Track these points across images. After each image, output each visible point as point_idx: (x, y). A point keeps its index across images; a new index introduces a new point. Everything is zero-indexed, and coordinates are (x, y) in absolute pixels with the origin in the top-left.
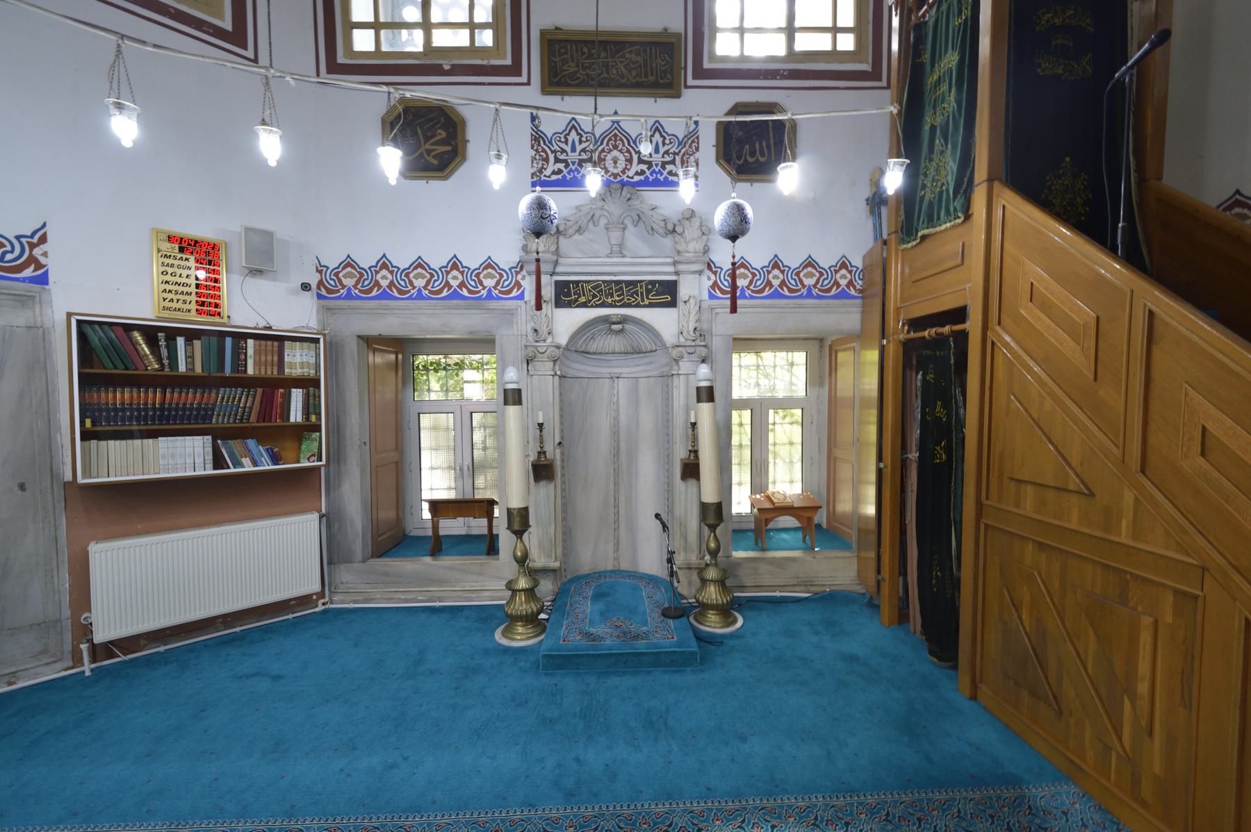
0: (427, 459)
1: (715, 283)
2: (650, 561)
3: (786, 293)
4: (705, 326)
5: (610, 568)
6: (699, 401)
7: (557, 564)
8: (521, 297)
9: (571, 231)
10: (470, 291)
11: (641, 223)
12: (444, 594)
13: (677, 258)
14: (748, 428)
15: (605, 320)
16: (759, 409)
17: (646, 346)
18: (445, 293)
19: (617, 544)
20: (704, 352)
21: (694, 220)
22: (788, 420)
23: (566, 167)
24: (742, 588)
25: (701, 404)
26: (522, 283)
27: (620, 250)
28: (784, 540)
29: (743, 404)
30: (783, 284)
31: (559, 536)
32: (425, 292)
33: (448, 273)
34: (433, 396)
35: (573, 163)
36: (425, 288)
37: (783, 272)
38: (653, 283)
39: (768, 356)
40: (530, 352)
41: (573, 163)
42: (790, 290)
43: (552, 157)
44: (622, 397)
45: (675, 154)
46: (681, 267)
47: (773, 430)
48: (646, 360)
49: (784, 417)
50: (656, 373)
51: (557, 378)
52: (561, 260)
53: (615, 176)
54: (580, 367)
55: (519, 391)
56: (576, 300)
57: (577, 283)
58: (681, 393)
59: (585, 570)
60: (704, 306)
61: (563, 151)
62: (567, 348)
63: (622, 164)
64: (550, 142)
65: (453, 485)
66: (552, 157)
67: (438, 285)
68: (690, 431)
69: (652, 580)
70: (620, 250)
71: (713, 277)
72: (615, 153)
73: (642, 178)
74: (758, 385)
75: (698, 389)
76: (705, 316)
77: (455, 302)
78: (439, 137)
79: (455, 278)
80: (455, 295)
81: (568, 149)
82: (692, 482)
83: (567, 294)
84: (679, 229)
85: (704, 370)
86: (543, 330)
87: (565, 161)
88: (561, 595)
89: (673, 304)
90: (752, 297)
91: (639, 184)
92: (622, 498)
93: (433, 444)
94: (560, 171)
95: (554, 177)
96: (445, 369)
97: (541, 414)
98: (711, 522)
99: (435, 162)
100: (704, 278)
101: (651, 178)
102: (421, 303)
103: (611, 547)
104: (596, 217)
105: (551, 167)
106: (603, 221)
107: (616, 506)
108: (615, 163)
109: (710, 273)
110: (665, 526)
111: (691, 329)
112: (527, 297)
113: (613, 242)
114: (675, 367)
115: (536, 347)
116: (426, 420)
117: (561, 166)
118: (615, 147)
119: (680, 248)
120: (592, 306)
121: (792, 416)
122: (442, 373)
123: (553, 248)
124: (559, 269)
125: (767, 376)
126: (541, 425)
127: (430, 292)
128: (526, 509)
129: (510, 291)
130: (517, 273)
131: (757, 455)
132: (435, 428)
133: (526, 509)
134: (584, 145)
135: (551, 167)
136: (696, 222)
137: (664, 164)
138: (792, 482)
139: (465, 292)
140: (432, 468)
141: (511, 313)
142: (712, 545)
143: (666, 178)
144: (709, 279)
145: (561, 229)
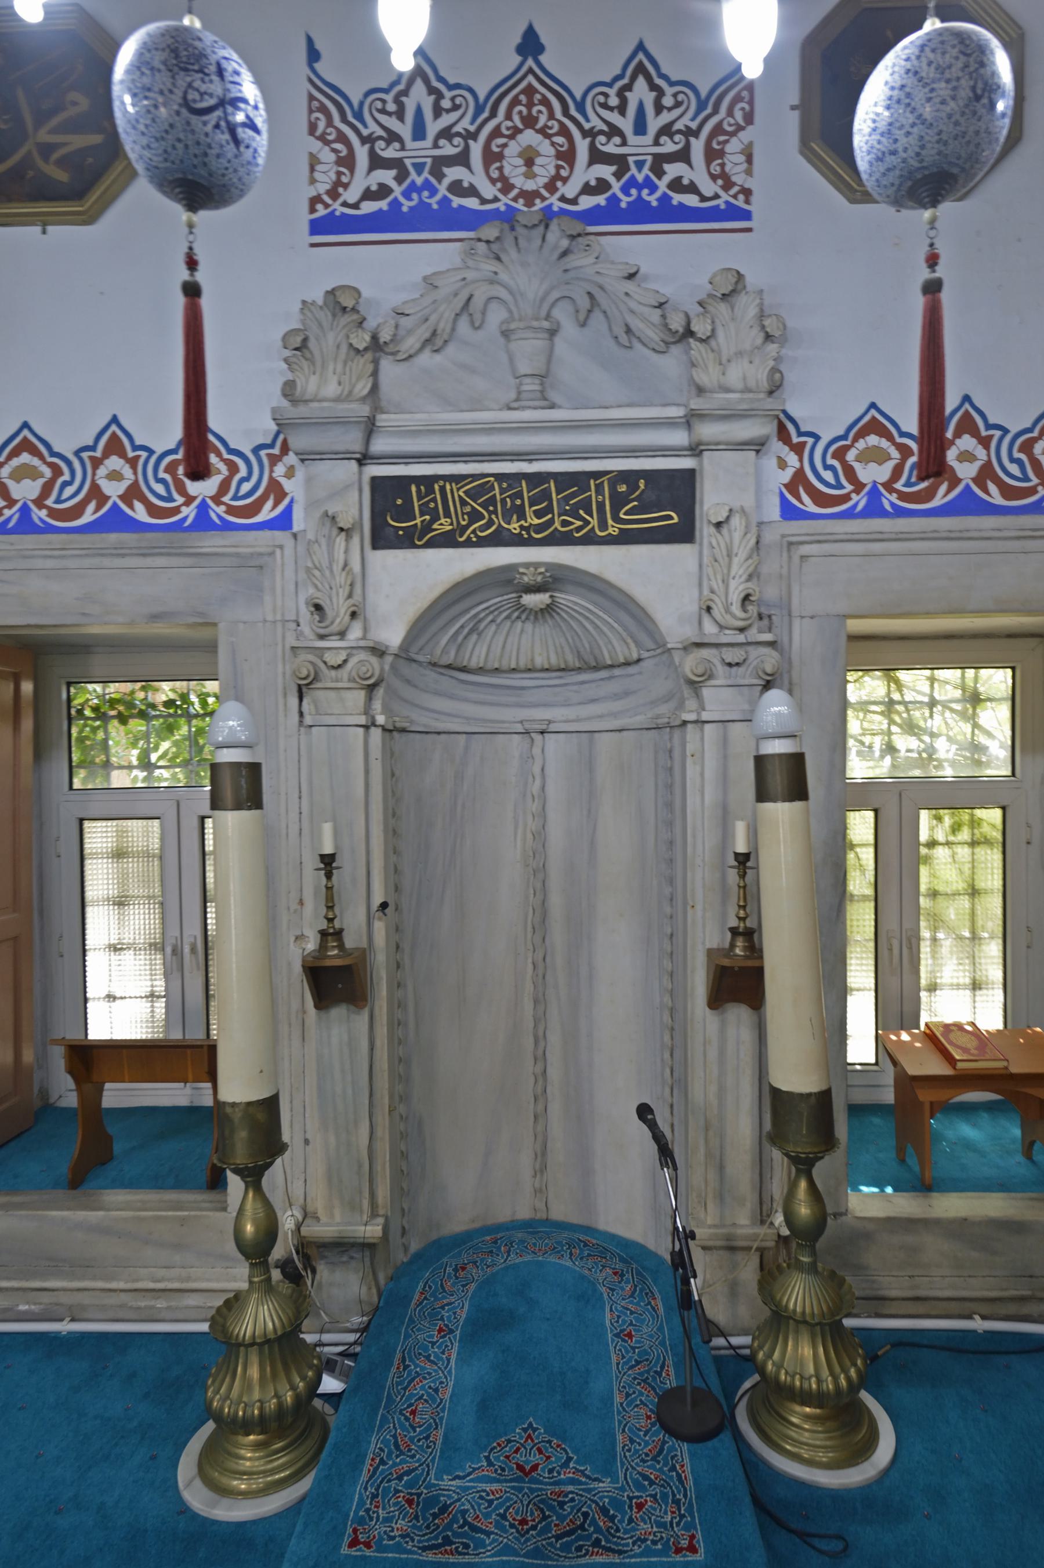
0: (100, 928)
1: (799, 476)
2: (627, 1202)
3: (996, 497)
4: (771, 592)
5: (524, 1213)
6: (762, 795)
7: (373, 1231)
8: (284, 522)
9: (411, 343)
10: (153, 510)
11: (597, 316)
12: (85, 1299)
13: (696, 404)
14: (995, 904)
15: (503, 578)
16: (897, 803)
17: (618, 648)
18: (89, 516)
19: (542, 1154)
20: (770, 660)
21: (742, 300)
22: (965, 835)
23: (400, 179)
24: (878, 1304)
25: (768, 806)
26: (287, 485)
27: (543, 388)
28: (968, 1145)
29: (865, 795)
30: (986, 474)
31: (384, 1149)
32: (40, 515)
33: (97, 463)
34: (119, 779)
35: (419, 168)
36: (39, 502)
37: (985, 442)
38: (629, 477)
39: (915, 681)
40: (304, 664)
41: (419, 168)
42: (1007, 492)
43: (362, 154)
44: (552, 785)
45: (690, 133)
46: (707, 431)
47: (927, 859)
48: (614, 687)
49: (955, 829)
50: (639, 720)
51: (376, 734)
52: (382, 420)
53: (529, 197)
54: (443, 706)
55: (254, 769)
56: (427, 528)
57: (428, 481)
58: (711, 774)
59: (458, 1224)
60: (770, 537)
61: (392, 137)
62: (405, 654)
63: (546, 166)
64: (359, 116)
65: (160, 986)
66: (362, 154)
67: (70, 496)
68: (733, 876)
69: (626, 1255)
70: (543, 388)
71: (792, 459)
72: (529, 137)
73: (601, 200)
74: (890, 749)
75: (760, 761)
76: (772, 565)
77: (113, 537)
78: (71, 112)
79: (115, 476)
80: (116, 521)
81: (405, 130)
82: (739, 1014)
83: (400, 514)
84: (700, 328)
85: (776, 707)
86: (338, 608)
87: (396, 164)
88: (385, 1315)
89: (683, 533)
90: (899, 513)
91: (592, 216)
92: (554, 1039)
93: (113, 892)
94: (383, 191)
95: (369, 207)
96: (143, 715)
97: (327, 828)
98: (803, 1149)
99: (62, 176)
100: (770, 463)
101: (625, 201)
102: (29, 541)
103: (526, 1161)
104: (478, 302)
105: (362, 180)
106: (496, 316)
107: (541, 1058)
108: (529, 163)
109: (784, 451)
110: (665, 1153)
111: (735, 597)
112: (298, 525)
113: (524, 368)
114: (691, 704)
115: (320, 652)
116: (99, 836)
117: (387, 176)
118: (530, 122)
119: (704, 378)
120: (468, 544)
121: (974, 823)
122: (137, 725)
123: (363, 387)
124: (380, 445)
125: (911, 728)
126: (328, 861)
127: (53, 513)
128: (271, 1104)
129: (255, 508)
130: (274, 460)
131: (890, 923)
132: (119, 854)
133: (271, 1104)
134: (446, 120)
135: (362, 180)
136: (747, 307)
137: (659, 162)
138: (976, 986)
139: (140, 513)
140: (115, 948)
141: (259, 564)
142: (804, 1210)
143: (665, 199)
144: (782, 464)
145: (385, 336)
